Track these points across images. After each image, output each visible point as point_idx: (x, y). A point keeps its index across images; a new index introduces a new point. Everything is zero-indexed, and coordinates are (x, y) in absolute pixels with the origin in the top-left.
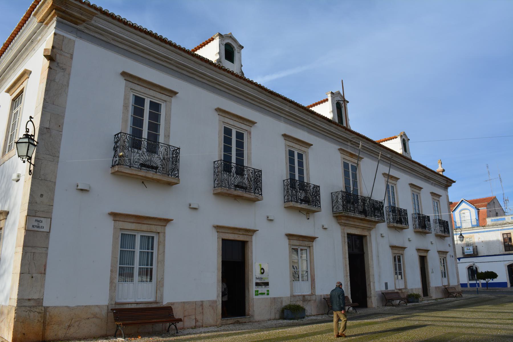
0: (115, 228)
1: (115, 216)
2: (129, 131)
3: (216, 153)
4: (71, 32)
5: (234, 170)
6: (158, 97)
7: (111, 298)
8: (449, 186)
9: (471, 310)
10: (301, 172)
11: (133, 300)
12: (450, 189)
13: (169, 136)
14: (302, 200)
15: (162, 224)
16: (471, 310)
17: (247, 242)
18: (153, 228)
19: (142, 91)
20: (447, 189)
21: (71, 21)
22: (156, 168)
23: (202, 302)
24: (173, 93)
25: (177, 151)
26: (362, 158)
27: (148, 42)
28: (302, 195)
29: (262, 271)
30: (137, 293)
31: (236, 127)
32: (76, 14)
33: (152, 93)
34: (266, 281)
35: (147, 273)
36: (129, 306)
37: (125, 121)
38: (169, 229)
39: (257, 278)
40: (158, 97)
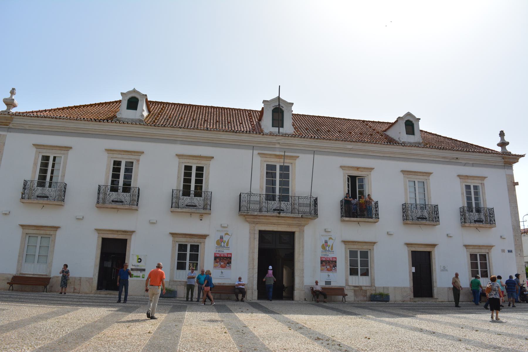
0: (23, 233)
1: (22, 226)
2: (466, 205)
3: (462, 202)
4: (4, 131)
5: (474, 210)
6: (422, 178)
7: (18, 271)
8: (515, 163)
9: (457, 321)
10: (477, 199)
11: (33, 273)
12: (515, 166)
13: (64, 176)
14: (475, 221)
15: (55, 229)
16: (457, 321)
17: (127, 240)
18: (48, 232)
19: (413, 177)
20: (511, 168)
21: (4, 125)
22: (426, 218)
23: (81, 278)
24: (429, 174)
25: (436, 206)
26: (298, 157)
27: (49, 122)
28: (475, 216)
29: (139, 260)
30: (32, 270)
31: (472, 183)
32: (3, 121)
33: (473, 181)
34: (143, 268)
35: (365, 273)
36: (28, 276)
37: (34, 172)
38: (58, 232)
39: (132, 265)
40: (477, 183)
